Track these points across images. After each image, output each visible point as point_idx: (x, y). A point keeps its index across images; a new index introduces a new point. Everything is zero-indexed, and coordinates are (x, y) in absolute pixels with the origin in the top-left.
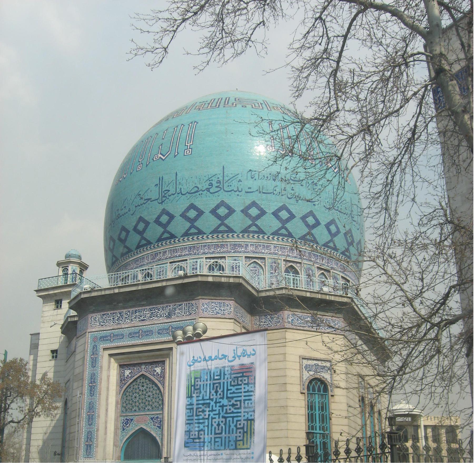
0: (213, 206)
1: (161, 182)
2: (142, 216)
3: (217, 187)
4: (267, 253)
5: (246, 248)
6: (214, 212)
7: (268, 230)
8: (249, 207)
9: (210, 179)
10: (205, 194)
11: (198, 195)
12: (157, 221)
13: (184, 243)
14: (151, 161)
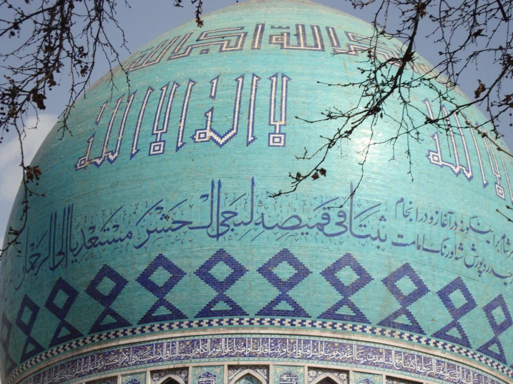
0: (329, 263)
1: (216, 191)
2: (166, 254)
3: (339, 224)
6: (329, 274)
9: (326, 206)
10: (314, 234)
11: (300, 235)
12: (204, 273)
13: (263, 328)
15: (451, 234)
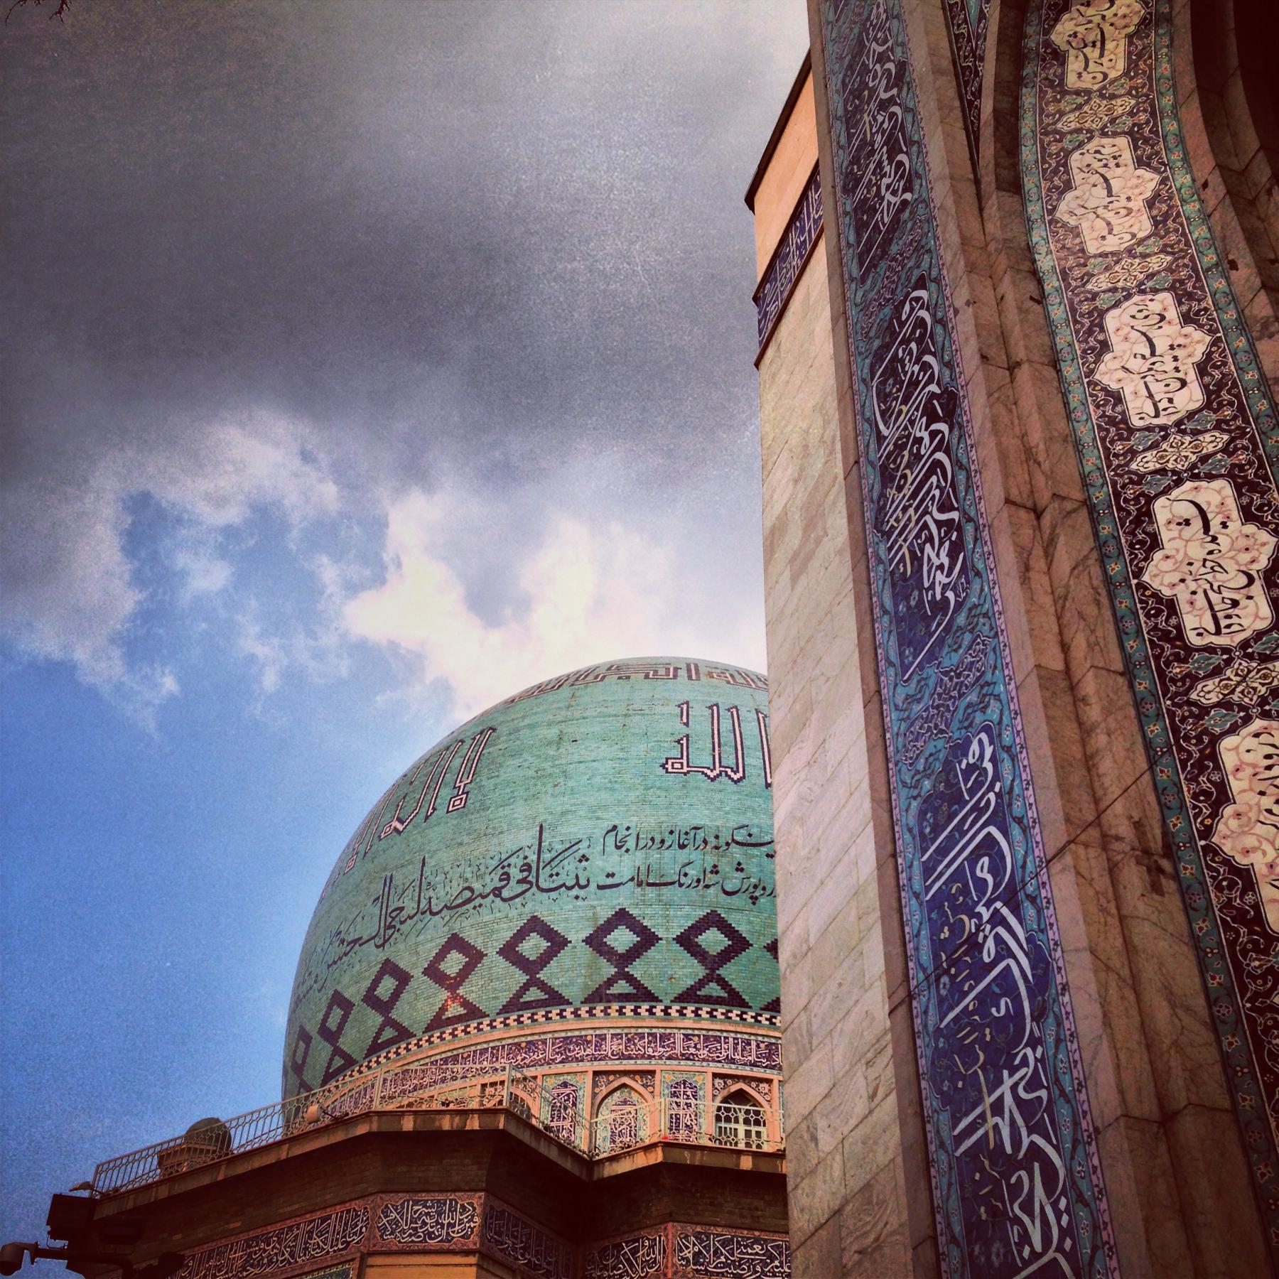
4: (660, 1058)
5: (598, 1047)
7: (665, 989)
8: (609, 926)
9: (505, 863)
14: (376, 840)
15: (695, 856)
